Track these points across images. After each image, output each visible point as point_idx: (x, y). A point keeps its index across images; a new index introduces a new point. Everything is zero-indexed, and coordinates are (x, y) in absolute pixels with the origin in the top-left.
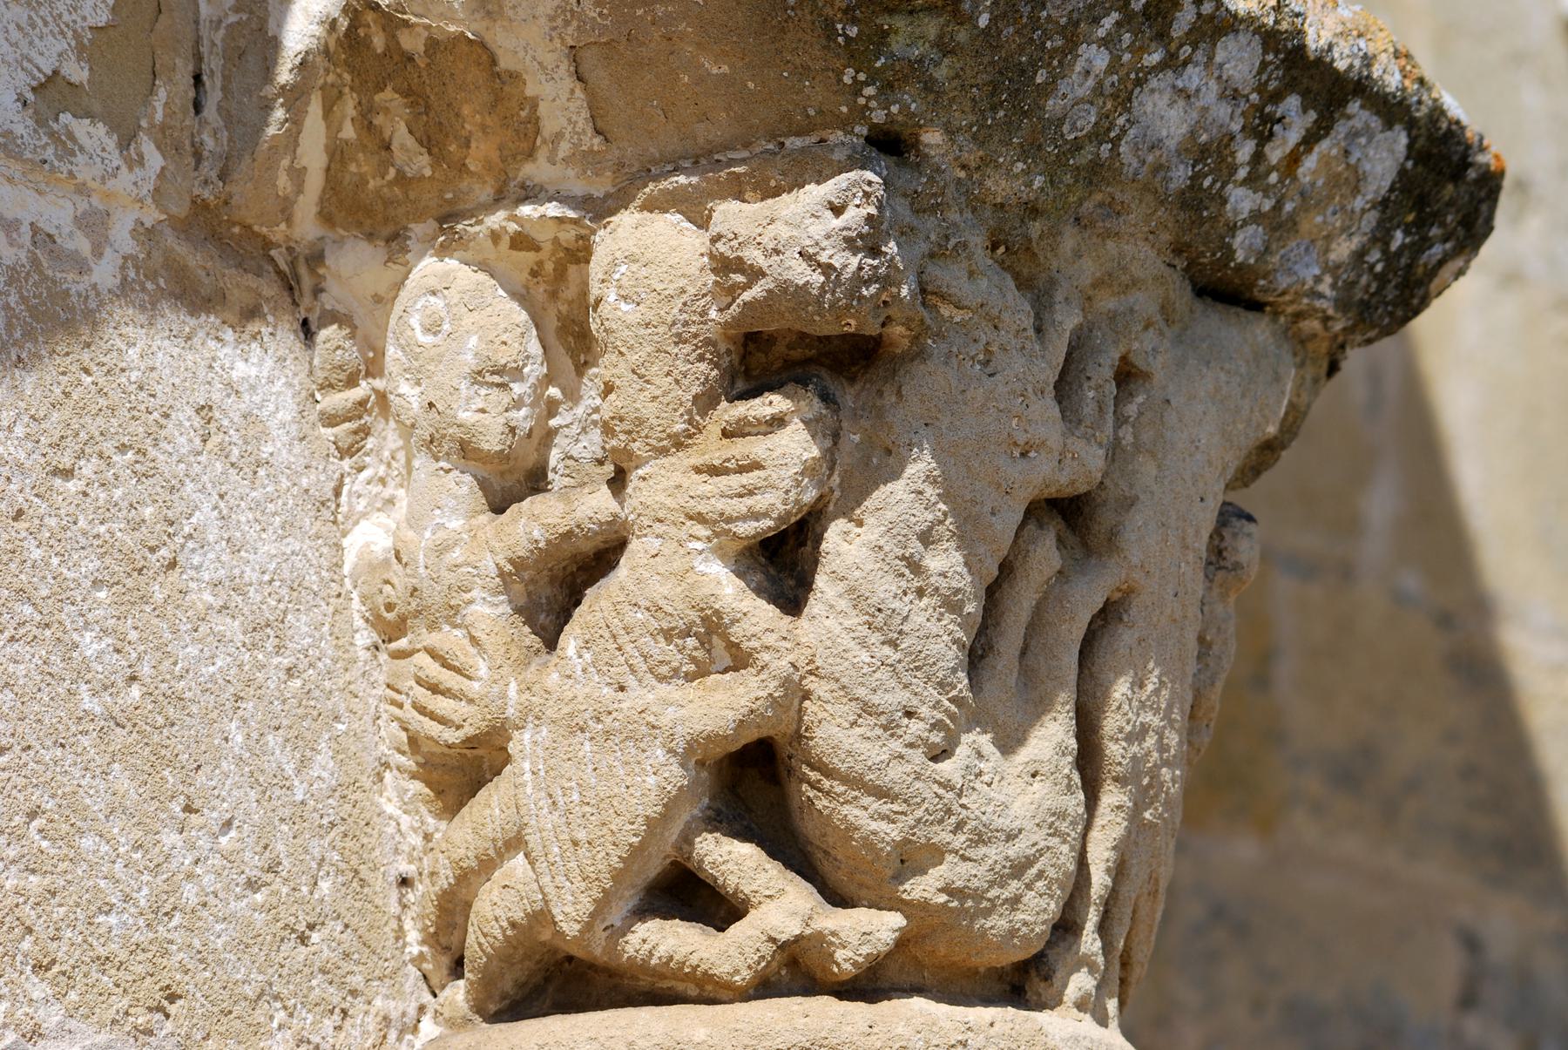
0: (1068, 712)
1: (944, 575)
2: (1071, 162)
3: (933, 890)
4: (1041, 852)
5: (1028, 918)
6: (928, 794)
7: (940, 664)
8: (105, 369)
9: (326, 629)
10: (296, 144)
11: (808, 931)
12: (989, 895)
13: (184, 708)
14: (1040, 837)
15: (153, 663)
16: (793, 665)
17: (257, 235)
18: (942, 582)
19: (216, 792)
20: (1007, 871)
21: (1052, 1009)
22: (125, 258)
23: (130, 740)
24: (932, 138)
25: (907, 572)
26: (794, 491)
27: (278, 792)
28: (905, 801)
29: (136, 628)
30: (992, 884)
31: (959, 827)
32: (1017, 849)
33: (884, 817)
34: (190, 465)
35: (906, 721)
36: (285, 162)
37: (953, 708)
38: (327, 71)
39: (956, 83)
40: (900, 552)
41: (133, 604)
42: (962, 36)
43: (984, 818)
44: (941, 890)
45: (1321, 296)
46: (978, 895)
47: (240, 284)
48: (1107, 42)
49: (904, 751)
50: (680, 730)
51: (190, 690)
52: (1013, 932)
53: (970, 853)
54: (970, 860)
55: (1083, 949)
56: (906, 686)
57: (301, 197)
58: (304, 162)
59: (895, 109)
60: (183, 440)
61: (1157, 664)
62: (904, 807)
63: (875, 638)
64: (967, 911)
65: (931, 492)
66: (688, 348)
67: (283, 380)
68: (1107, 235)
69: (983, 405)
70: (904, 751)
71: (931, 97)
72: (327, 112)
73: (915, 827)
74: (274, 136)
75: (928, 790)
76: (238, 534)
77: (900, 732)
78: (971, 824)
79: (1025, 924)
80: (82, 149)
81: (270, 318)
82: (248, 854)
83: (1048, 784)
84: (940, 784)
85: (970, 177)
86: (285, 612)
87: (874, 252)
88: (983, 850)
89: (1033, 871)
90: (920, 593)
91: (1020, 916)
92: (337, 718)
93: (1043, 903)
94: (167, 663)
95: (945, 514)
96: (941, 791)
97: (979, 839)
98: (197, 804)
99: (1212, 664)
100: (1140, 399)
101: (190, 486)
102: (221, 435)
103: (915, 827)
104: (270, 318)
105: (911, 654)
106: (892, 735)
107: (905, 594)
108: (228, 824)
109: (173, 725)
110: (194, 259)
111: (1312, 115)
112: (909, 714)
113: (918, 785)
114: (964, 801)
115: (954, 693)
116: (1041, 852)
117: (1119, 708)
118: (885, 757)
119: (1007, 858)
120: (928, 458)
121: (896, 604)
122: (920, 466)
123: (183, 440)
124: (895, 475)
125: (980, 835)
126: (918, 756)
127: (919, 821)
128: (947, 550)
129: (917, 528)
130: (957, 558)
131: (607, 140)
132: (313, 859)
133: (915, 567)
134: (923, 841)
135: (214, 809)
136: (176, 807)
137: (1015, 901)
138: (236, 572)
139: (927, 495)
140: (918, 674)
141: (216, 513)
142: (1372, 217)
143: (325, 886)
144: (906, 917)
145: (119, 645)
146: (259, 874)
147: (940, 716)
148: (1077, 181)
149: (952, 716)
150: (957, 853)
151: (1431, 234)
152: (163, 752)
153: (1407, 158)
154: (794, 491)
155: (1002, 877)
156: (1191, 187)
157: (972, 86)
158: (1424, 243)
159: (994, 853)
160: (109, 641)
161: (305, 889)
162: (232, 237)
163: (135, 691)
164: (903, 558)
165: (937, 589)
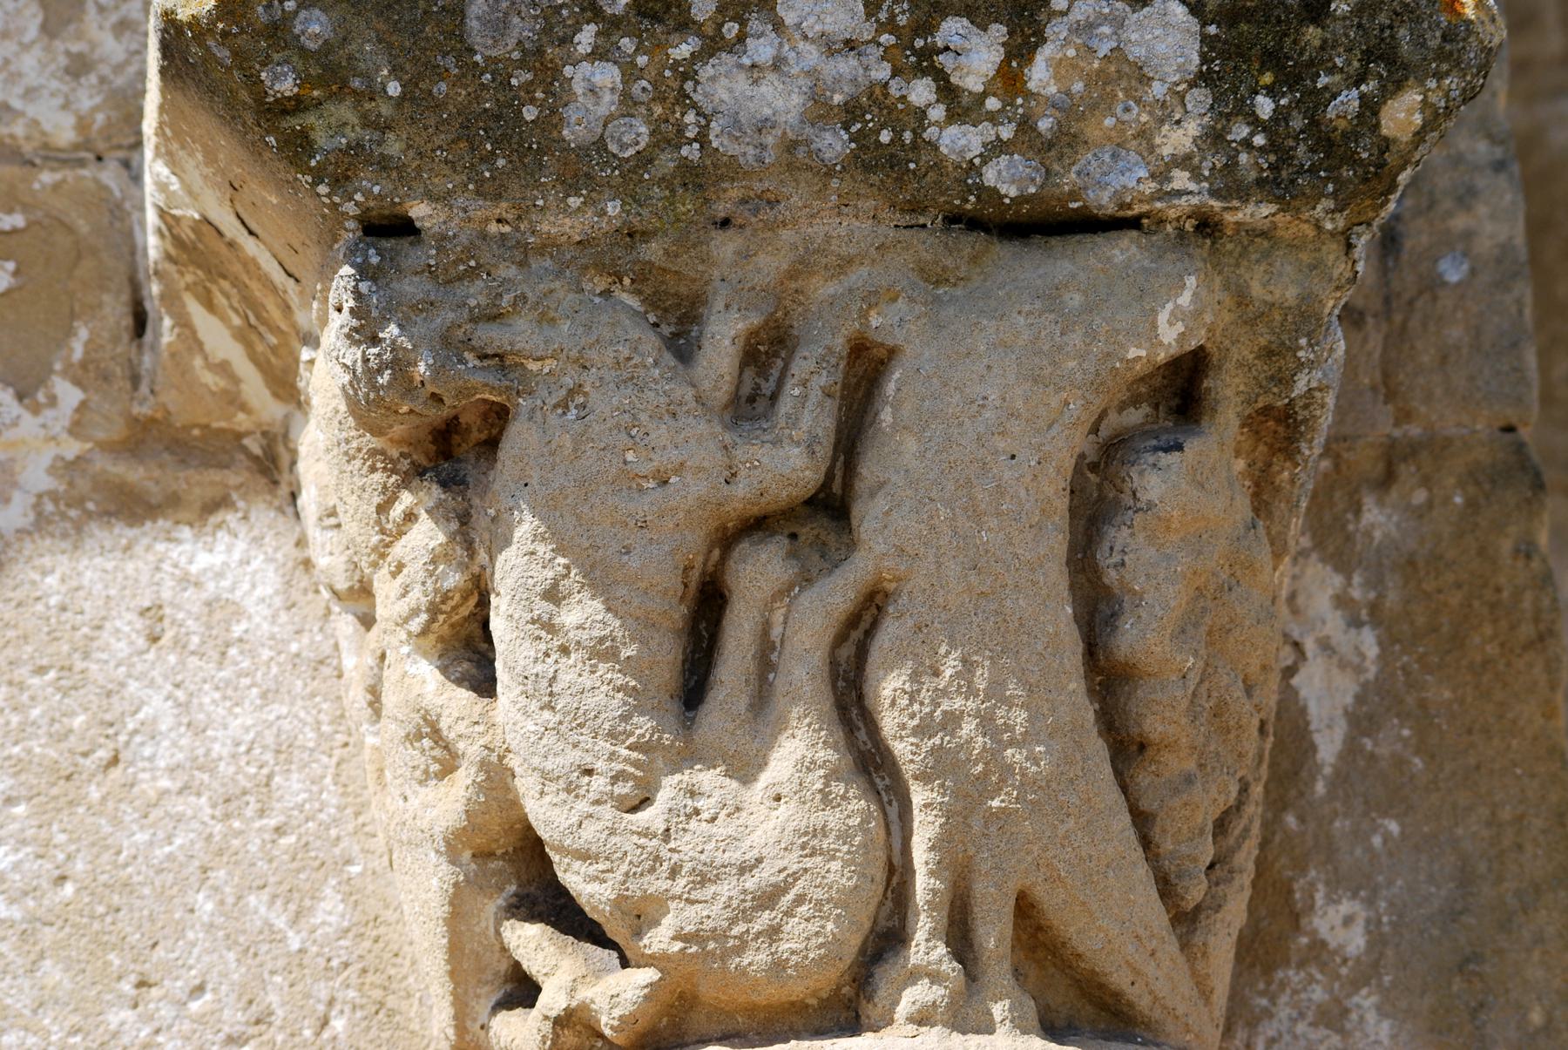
0: (809, 725)
1: (580, 627)
2: (646, 176)
3: (667, 940)
4: (795, 876)
5: (794, 946)
6: (628, 847)
7: (603, 716)
8: (13, 604)
9: (328, 780)
11: (574, 1004)
12: (733, 933)
13: (131, 892)
14: (792, 862)
15: (89, 858)
16: (486, 747)
17: (221, 431)
18: (584, 636)
19: (180, 962)
20: (748, 904)
21: (876, 1029)
22: (40, 496)
23: (61, 935)
24: (419, 211)
25: (543, 634)
26: (429, 581)
27: (264, 948)
28: (607, 859)
29: (64, 831)
30: (733, 921)
31: (674, 872)
32: (765, 875)
33: (595, 879)
34: (133, 665)
35: (587, 779)
36: (198, 362)
37: (635, 755)
38: (182, 274)
39: (411, 153)
40: (528, 616)
41: (59, 810)
42: (386, 110)
43: (703, 857)
44: (674, 938)
45: (1179, 193)
46: (719, 935)
47: (199, 482)
49: (591, 809)
50: (437, 829)
51: (139, 873)
52: (778, 966)
53: (694, 895)
54: (698, 902)
55: (913, 960)
56: (575, 746)
59: (358, 197)
60: (122, 645)
61: (953, 646)
62: (607, 865)
63: (534, 705)
64: (713, 953)
65: (543, 550)
66: (358, 463)
67: (262, 557)
68: (772, 226)
69: (575, 450)
70: (591, 809)
71: (394, 174)
72: (210, 305)
73: (625, 882)
74: (170, 344)
75: (628, 843)
76: (201, 716)
77: (582, 792)
78: (687, 867)
79: (793, 953)
81: (241, 504)
82: (227, 1014)
83: (793, 804)
84: (639, 834)
85: (517, 229)
86: (270, 777)
87: (375, 340)
88: (711, 889)
89: (790, 896)
90: (564, 650)
91: (784, 946)
92: (348, 862)
93: (813, 927)
94: (106, 857)
95: (567, 567)
96: (643, 841)
97: (703, 879)
98: (153, 979)
99: (1144, 615)
100: (897, 375)
101: (133, 686)
102: (175, 629)
103: (625, 882)
104: (241, 504)
105: (569, 713)
106: (577, 796)
107: (547, 655)
108: (199, 989)
109: (118, 910)
110: (134, 474)
111: (999, 31)
112: (589, 772)
113: (614, 839)
114: (672, 845)
115: (632, 740)
116: (795, 876)
117: (893, 703)
118: (574, 820)
119: (744, 892)
120: (528, 517)
121: (539, 668)
122: (526, 527)
123: (122, 645)
124: (507, 542)
125: (701, 874)
126: (607, 812)
127: (627, 874)
128: (580, 601)
129: (538, 589)
130: (597, 605)
131: (297, 280)
132: (319, 1001)
133: (550, 627)
134: (639, 893)
135: (177, 979)
136: (127, 987)
137: (773, 933)
138: (201, 751)
139: (540, 553)
140: (584, 731)
141: (170, 703)
142: (1200, 98)
143: (338, 1024)
144: (661, 971)
145: (41, 851)
146: (243, 1028)
147: (620, 767)
148: (673, 191)
149: (636, 764)
150: (680, 897)
151: (1319, 86)
152: (106, 938)
153: (1204, 24)
154: (429, 581)
155: (744, 912)
156: (861, 148)
157: (433, 151)
158: (1315, 102)
159: (727, 889)
160: (29, 849)
161: (307, 1033)
162: (195, 439)
163: (69, 889)
164: (533, 622)
165: (578, 643)
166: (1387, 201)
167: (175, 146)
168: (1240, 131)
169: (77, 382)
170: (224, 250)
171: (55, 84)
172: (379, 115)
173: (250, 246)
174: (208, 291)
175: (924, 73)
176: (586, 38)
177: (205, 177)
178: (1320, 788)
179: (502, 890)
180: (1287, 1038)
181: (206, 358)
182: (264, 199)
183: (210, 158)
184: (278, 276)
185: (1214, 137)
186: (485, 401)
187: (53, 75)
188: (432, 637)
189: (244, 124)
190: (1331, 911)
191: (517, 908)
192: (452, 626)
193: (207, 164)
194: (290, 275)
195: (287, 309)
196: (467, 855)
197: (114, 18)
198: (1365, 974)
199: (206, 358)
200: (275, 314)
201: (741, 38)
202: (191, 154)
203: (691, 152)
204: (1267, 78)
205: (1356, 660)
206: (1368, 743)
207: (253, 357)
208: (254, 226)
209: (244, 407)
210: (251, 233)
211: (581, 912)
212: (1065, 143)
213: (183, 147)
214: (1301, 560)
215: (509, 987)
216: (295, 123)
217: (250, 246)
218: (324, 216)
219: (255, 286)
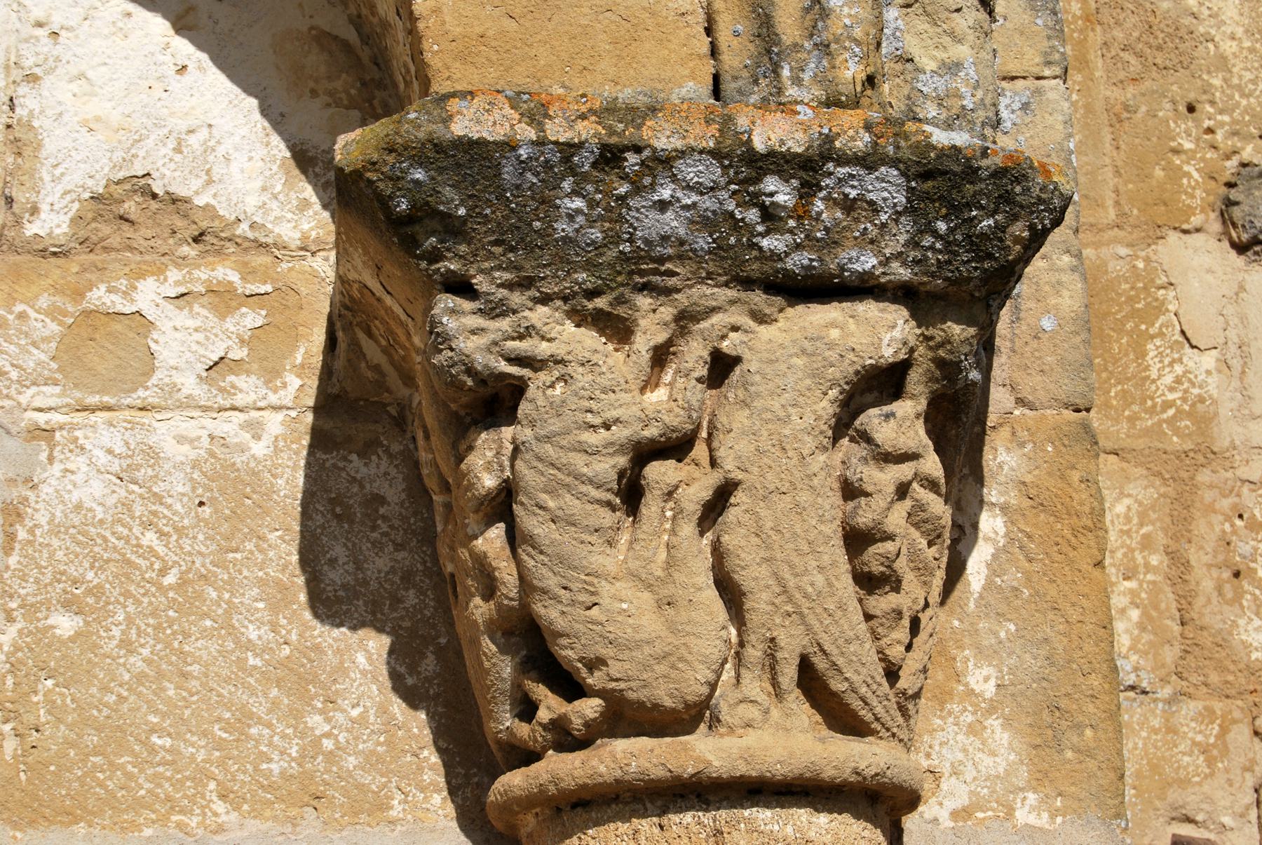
10: (364, 355)
17: (376, 402)
36: (363, 365)
48: (575, 193)
57: (387, 378)
58: (376, 361)
80: (241, 391)
153: (909, 181)
166: (1010, 281)
167: (347, 246)
168: (927, 241)
169: (298, 376)
170: (376, 303)
171: (289, 216)
172: (454, 226)
173: (388, 300)
174: (369, 327)
175: (755, 205)
176: (567, 185)
177: (364, 263)
178: (972, 605)
179: (518, 653)
180: (951, 742)
181: (367, 362)
182: (393, 274)
183: (366, 253)
184: (403, 317)
185: (913, 243)
186: (512, 385)
187: (289, 211)
188: (481, 514)
189: (381, 231)
190: (977, 672)
191: (526, 663)
192: (492, 508)
193: (364, 255)
194: (409, 316)
195: (409, 335)
196: (499, 634)
197: (323, 180)
198: (991, 710)
199: (367, 362)
200: (403, 338)
201: (653, 185)
202: (356, 249)
203: (626, 247)
204: (944, 211)
205: (993, 536)
206: (998, 580)
207: (392, 362)
208: (389, 289)
209: (388, 390)
210: (388, 293)
211: (560, 666)
212: (832, 242)
213: (351, 246)
214: (963, 481)
215: (522, 707)
216: (409, 230)
217: (388, 300)
218: (424, 282)
219: (392, 323)
